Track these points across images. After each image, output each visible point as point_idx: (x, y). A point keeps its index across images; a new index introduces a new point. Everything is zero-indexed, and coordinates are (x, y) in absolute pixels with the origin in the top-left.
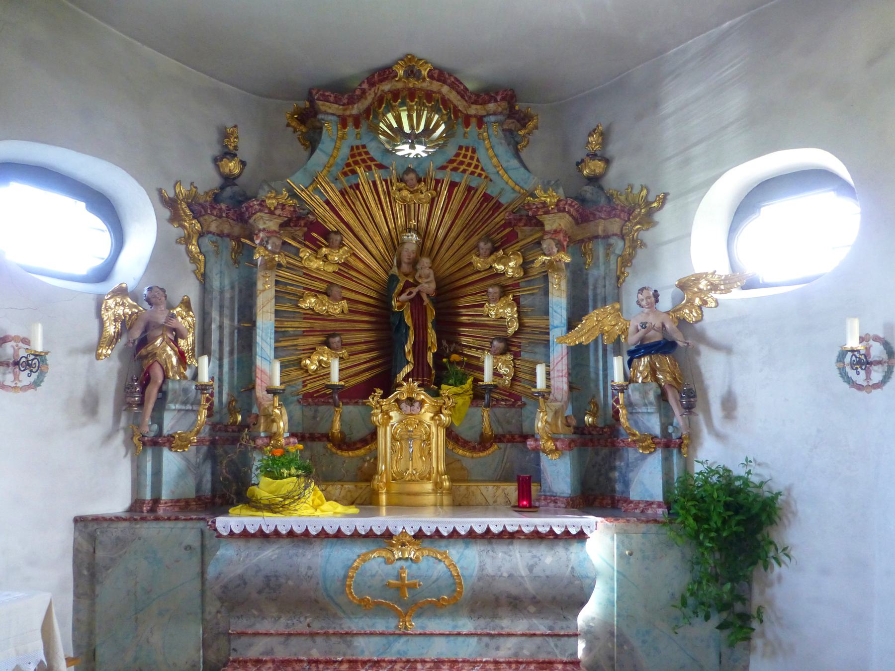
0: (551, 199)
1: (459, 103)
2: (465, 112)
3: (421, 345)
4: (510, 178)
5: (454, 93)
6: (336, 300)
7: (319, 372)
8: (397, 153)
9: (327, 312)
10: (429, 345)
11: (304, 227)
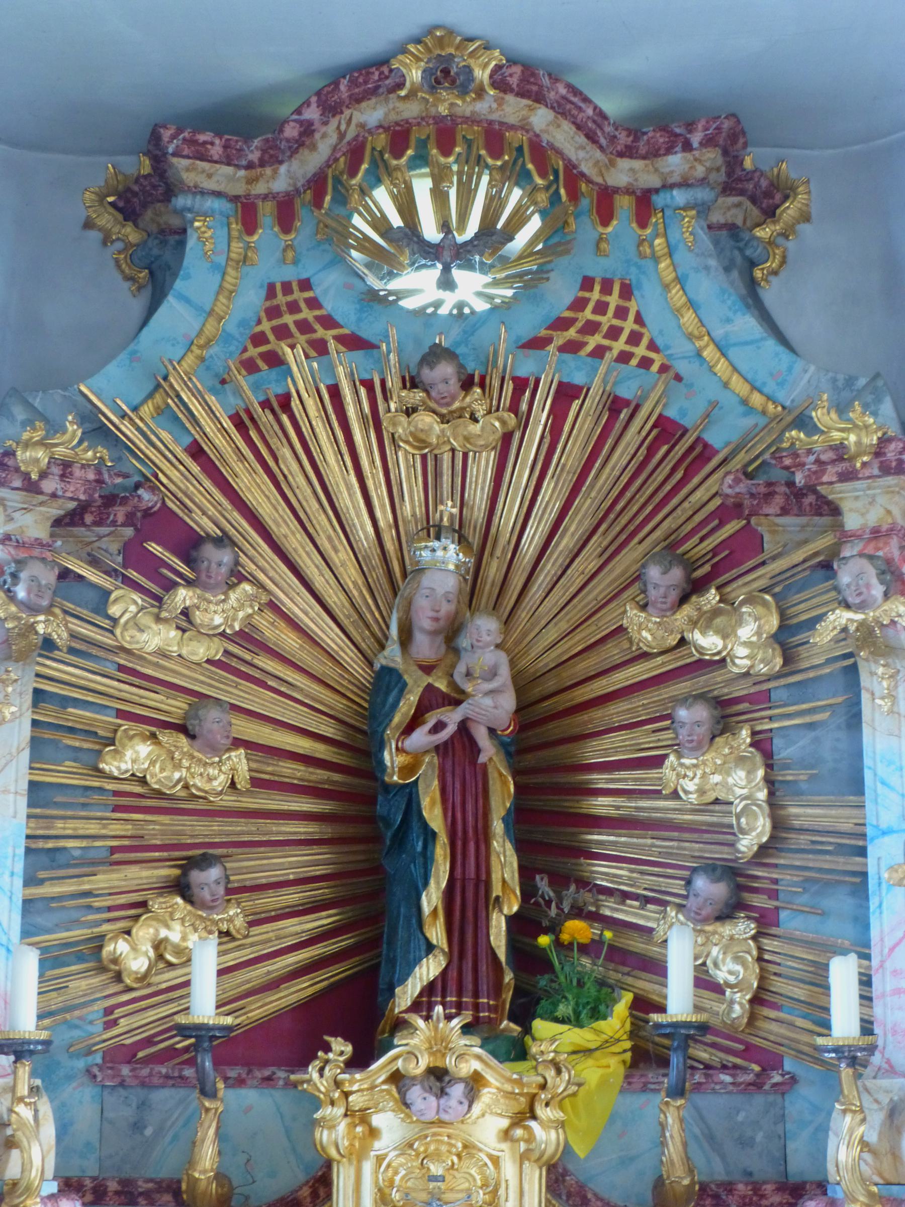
0: (858, 436)
1: (582, 154)
2: (599, 180)
3: (470, 894)
4: (735, 369)
5: (567, 126)
6: (214, 749)
7: (155, 979)
8: (402, 303)
9: (186, 787)
10: (497, 891)
11: (123, 525)
